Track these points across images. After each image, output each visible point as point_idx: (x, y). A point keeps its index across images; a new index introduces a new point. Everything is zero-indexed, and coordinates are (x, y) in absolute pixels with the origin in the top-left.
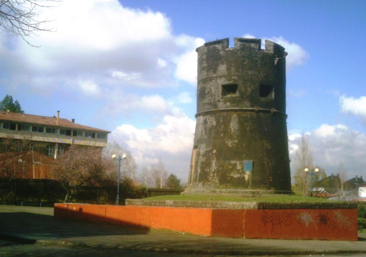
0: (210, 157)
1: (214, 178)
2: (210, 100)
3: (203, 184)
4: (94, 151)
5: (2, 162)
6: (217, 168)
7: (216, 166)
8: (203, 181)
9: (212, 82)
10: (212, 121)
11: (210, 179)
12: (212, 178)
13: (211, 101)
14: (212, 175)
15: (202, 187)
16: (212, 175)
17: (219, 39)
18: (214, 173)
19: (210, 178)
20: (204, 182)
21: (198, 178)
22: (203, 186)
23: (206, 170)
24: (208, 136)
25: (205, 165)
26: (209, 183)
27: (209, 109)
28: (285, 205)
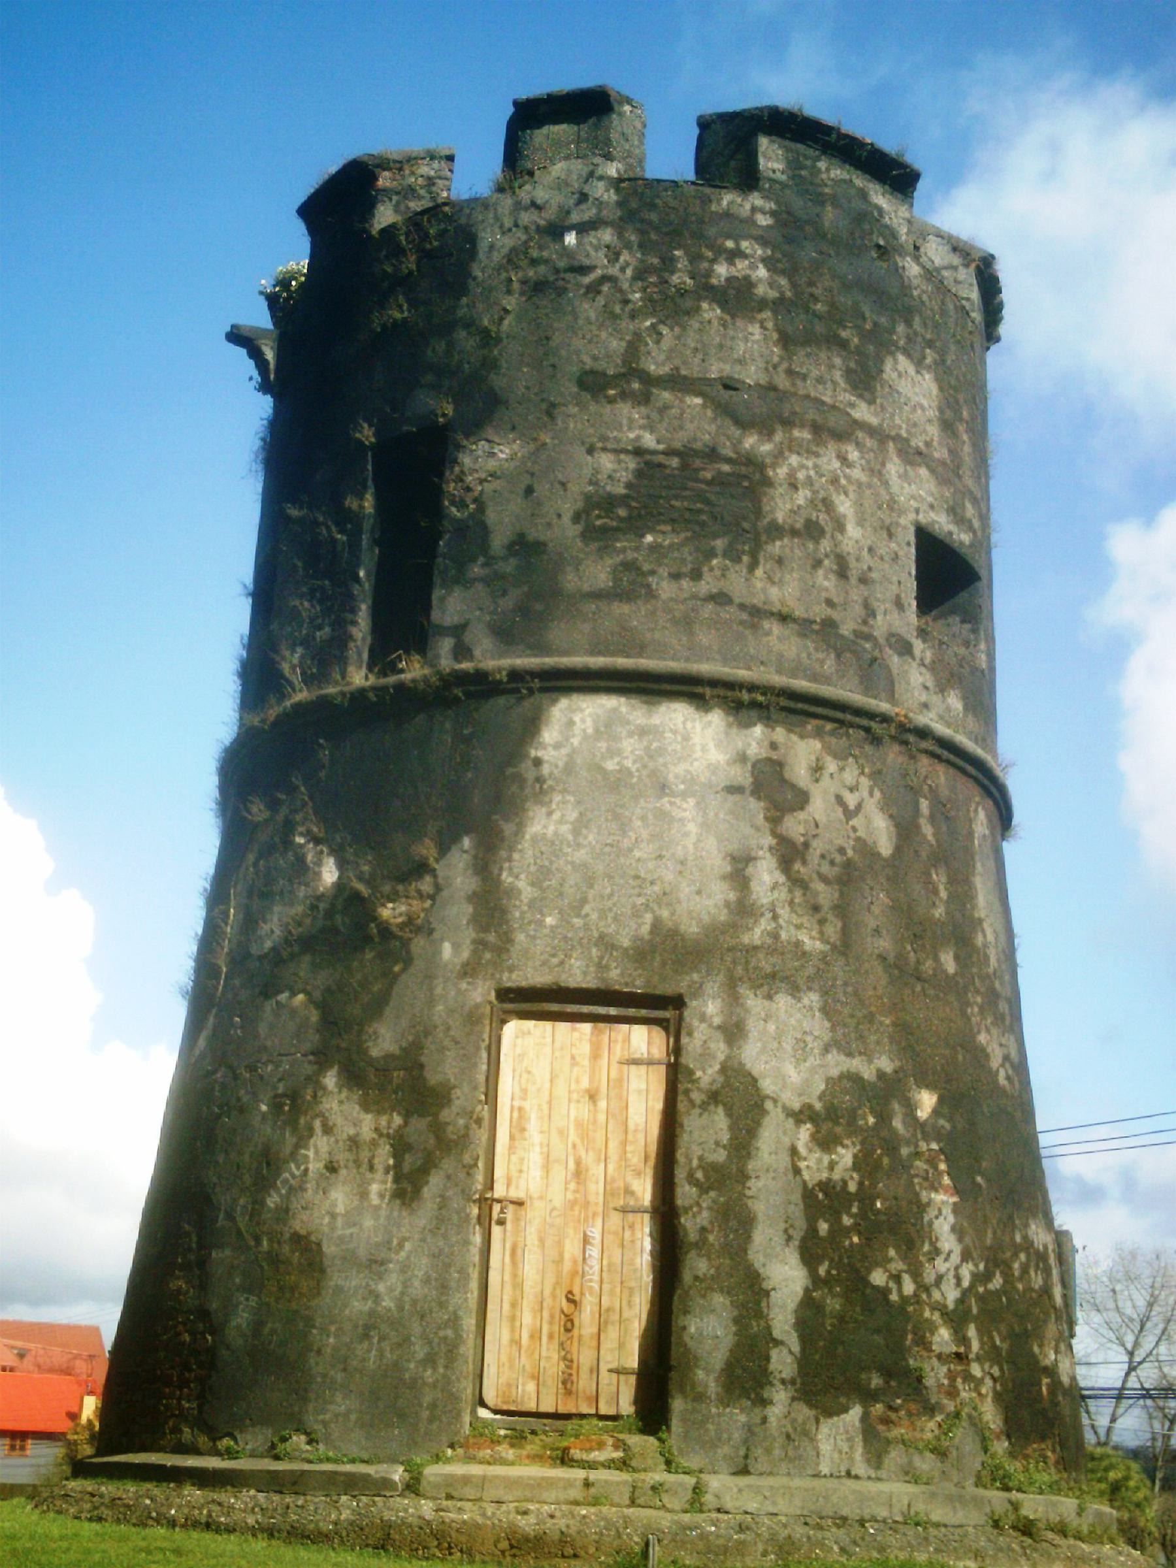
0: (905, 1151)
1: (968, 1377)
2: (829, 603)
3: (869, 1431)
4: (340, 1559)
5: (471, 342)
6: (977, 1278)
7: (966, 1256)
8: (868, 1397)
9: (843, 459)
10: (851, 800)
11: (929, 1382)
12: (952, 1376)
13: (835, 615)
14: (943, 1337)
15: (860, 1469)
16: (943, 1337)
17: (812, 110)
18: (957, 1319)
19: (935, 1374)
20: (878, 1408)
21: (783, 1363)
22: (876, 1458)
23: (878, 1278)
24: (833, 929)
25: (855, 1227)
26: (930, 1427)
27: (814, 678)
28: (736, 1313)
